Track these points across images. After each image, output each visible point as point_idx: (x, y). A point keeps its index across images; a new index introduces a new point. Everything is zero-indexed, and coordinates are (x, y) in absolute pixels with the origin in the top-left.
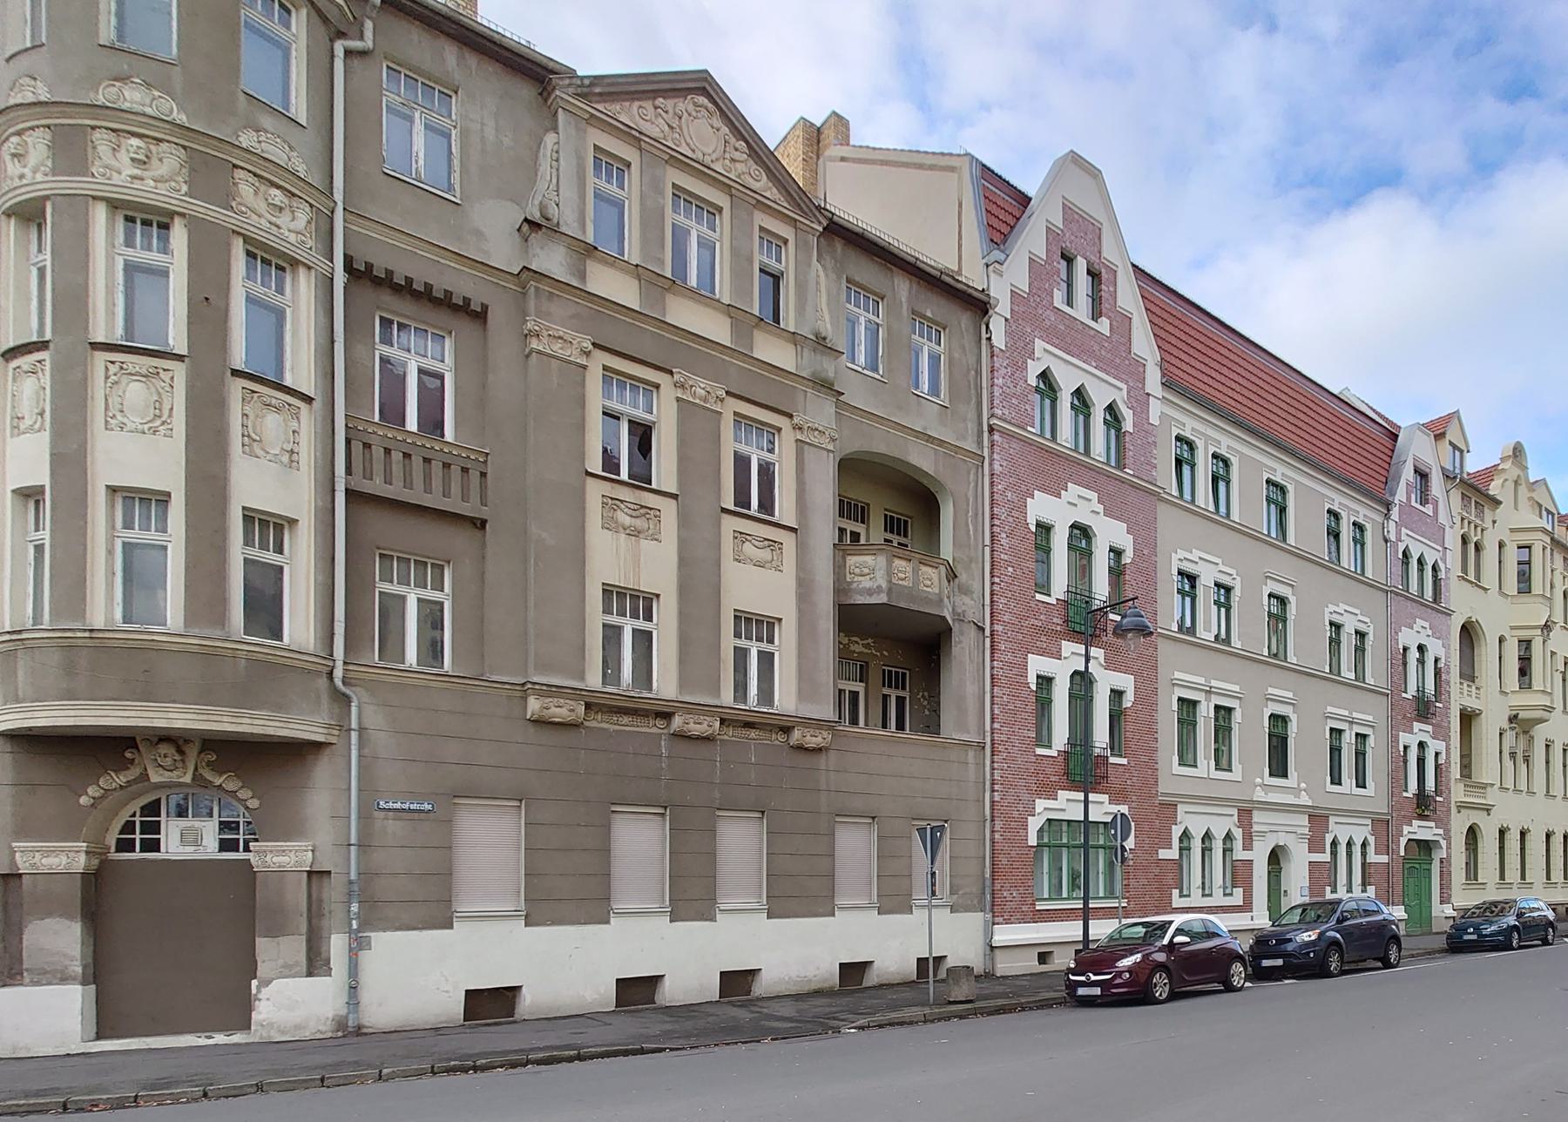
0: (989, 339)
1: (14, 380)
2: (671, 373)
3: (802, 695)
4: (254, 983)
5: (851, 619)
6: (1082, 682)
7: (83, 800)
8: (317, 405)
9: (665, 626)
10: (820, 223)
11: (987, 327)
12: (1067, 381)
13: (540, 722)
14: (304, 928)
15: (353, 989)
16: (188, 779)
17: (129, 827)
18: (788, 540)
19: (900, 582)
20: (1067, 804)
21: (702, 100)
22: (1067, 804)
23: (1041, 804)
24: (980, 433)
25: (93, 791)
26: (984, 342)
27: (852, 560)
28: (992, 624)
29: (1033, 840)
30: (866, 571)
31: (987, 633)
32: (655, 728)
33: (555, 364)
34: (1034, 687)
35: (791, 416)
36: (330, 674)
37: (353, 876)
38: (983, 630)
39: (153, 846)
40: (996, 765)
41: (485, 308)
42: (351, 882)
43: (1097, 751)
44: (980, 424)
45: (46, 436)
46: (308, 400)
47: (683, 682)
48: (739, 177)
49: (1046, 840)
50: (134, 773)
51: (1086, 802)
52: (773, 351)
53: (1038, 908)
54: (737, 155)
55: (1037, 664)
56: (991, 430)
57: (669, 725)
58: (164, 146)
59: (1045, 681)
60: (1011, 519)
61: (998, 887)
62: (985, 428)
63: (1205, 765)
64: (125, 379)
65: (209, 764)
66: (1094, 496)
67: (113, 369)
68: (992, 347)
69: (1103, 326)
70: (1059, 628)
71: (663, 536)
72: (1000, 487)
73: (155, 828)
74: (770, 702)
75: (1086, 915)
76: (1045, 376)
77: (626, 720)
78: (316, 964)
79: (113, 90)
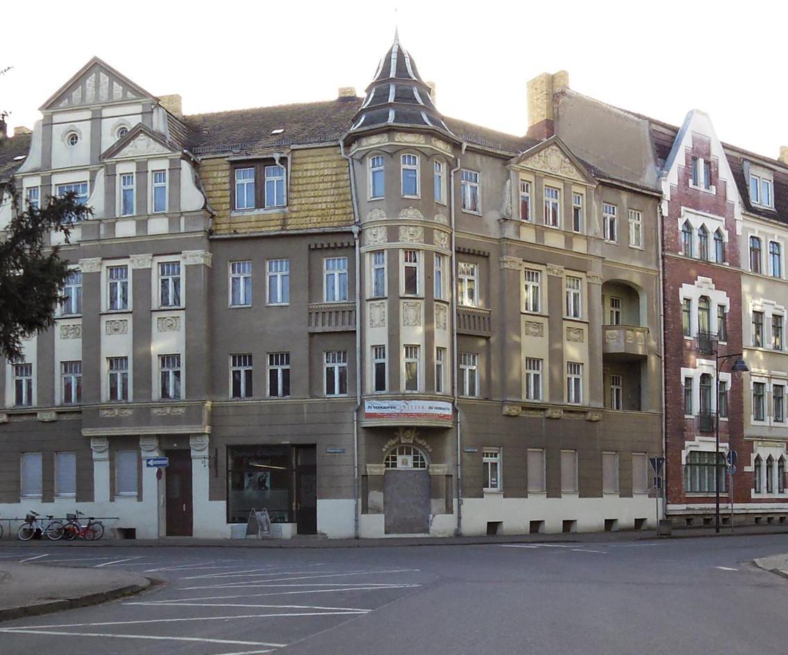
0: (661, 212)
1: (370, 309)
2: (546, 265)
3: (592, 397)
4: (431, 516)
7: (384, 450)
8: (450, 304)
10: (595, 184)
11: (660, 206)
12: (696, 222)
13: (508, 416)
14: (445, 496)
15: (459, 518)
16: (411, 442)
17: (387, 459)
18: (585, 327)
23: (687, 443)
24: (658, 259)
25: (386, 446)
26: (659, 214)
28: (665, 354)
30: (615, 337)
31: (663, 359)
32: (539, 415)
33: (511, 271)
35: (585, 272)
37: (459, 477)
38: (661, 357)
39: (394, 465)
41: (489, 253)
42: (458, 479)
44: (658, 256)
45: (386, 328)
46: (448, 303)
47: (551, 397)
48: (566, 174)
50: (397, 439)
52: (580, 246)
53: (687, 496)
56: (663, 257)
57: (544, 414)
58: (418, 228)
61: (668, 485)
62: (660, 257)
63: (769, 420)
65: (418, 436)
66: (710, 280)
67: (405, 305)
69: (713, 190)
73: (395, 459)
74: (578, 402)
76: (687, 223)
77: (531, 412)
78: (449, 510)
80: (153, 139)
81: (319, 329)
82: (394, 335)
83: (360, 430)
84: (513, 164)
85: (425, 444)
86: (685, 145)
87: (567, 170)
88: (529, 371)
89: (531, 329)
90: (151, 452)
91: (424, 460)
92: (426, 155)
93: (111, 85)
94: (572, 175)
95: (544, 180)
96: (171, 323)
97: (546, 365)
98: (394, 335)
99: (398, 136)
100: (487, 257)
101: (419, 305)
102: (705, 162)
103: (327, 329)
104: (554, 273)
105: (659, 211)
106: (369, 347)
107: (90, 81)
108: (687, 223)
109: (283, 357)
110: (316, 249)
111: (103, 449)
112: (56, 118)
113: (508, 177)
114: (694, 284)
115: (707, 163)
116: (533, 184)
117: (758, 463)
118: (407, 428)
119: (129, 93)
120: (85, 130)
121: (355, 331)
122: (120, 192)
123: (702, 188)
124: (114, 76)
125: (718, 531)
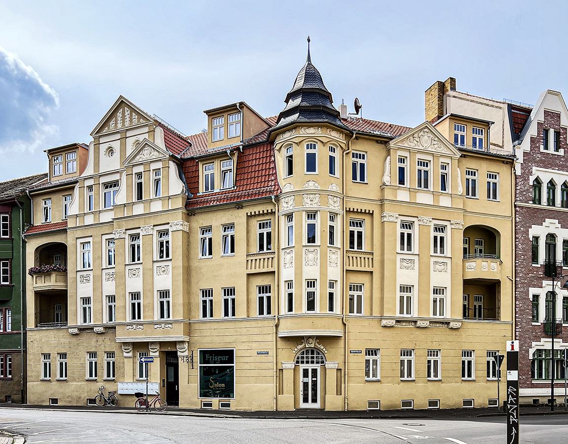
0: (515, 173)
5: (467, 283)
6: (552, 295)
9: (415, 294)
11: (514, 169)
12: (545, 176)
13: (385, 327)
17: (298, 358)
19: (484, 270)
20: (545, 344)
21: (426, 130)
22: (545, 344)
23: (534, 344)
27: (467, 264)
28: (515, 278)
29: (531, 357)
30: (473, 267)
34: (531, 300)
36: (343, 319)
40: (517, 330)
43: (557, 322)
48: (435, 149)
49: (536, 357)
50: (303, 345)
51: (553, 342)
54: (435, 143)
55: (533, 291)
59: (536, 297)
60: (523, 238)
64: (308, 253)
66: (556, 221)
67: (307, 251)
68: (516, 175)
69: (561, 152)
70: (541, 276)
71: (415, 268)
72: (519, 227)
75: (552, 386)
76: (537, 180)
79: (307, 184)
80: (153, 148)
81: (253, 271)
82: (299, 272)
83: (279, 339)
84: (392, 144)
85: (322, 347)
86: (536, 117)
87: (436, 146)
88: (205, 299)
89: (405, 264)
90: (154, 353)
91: (323, 359)
92: (322, 142)
93: (131, 115)
94: (441, 149)
95: (417, 154)
96: (163, 269)
97: (415, 291)
98: (299, 272)
99: (303, 130)
100: (372, 214)
101: (316, 251)
102: (555, 132)
103: (258, 271)
104: (424, 222)
105: (513, 172)
106: (283, 282)
107: (119, 115)
108: (537, 180)
109: (230, 291)
110: (251, 216)
111: (156, 350)
112: (102, 140)
113: (389, 154)
114: (542, 225)
115: (557, 134)
116: (408, 158)
117: (306, 392)
118: (310, 337)
119: (141, 120)
120: (116, 146)
121: (275, 271)
122: (135, 185)
123: (551, 150)
124: (133, 110)
125: (552, 410)
